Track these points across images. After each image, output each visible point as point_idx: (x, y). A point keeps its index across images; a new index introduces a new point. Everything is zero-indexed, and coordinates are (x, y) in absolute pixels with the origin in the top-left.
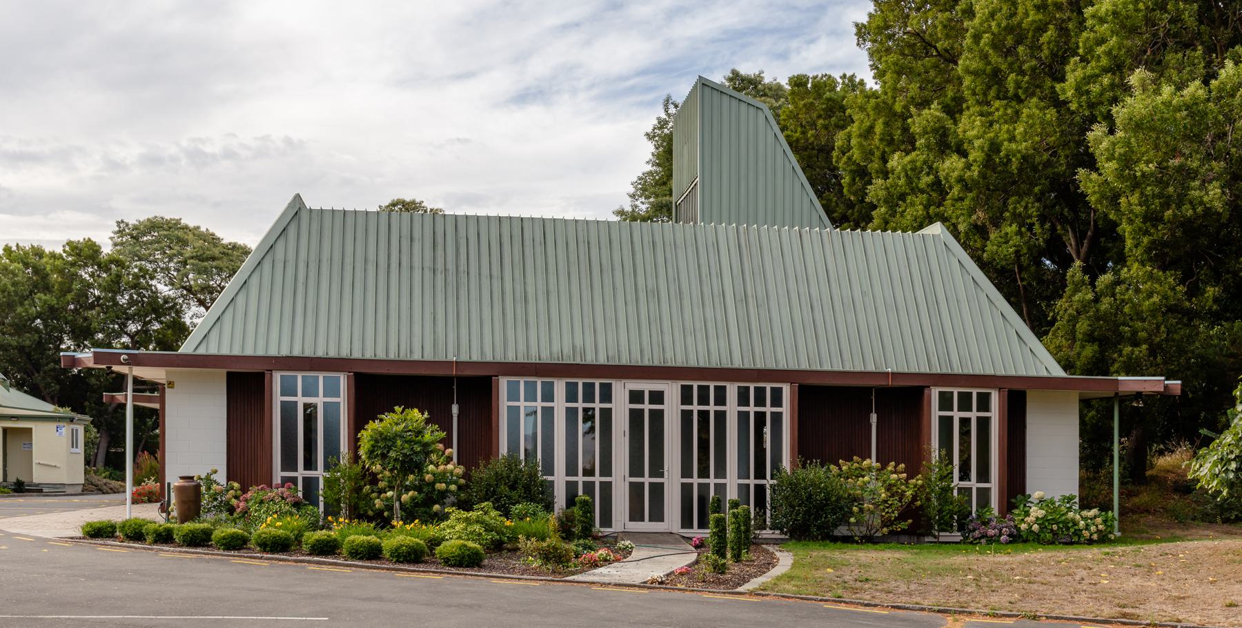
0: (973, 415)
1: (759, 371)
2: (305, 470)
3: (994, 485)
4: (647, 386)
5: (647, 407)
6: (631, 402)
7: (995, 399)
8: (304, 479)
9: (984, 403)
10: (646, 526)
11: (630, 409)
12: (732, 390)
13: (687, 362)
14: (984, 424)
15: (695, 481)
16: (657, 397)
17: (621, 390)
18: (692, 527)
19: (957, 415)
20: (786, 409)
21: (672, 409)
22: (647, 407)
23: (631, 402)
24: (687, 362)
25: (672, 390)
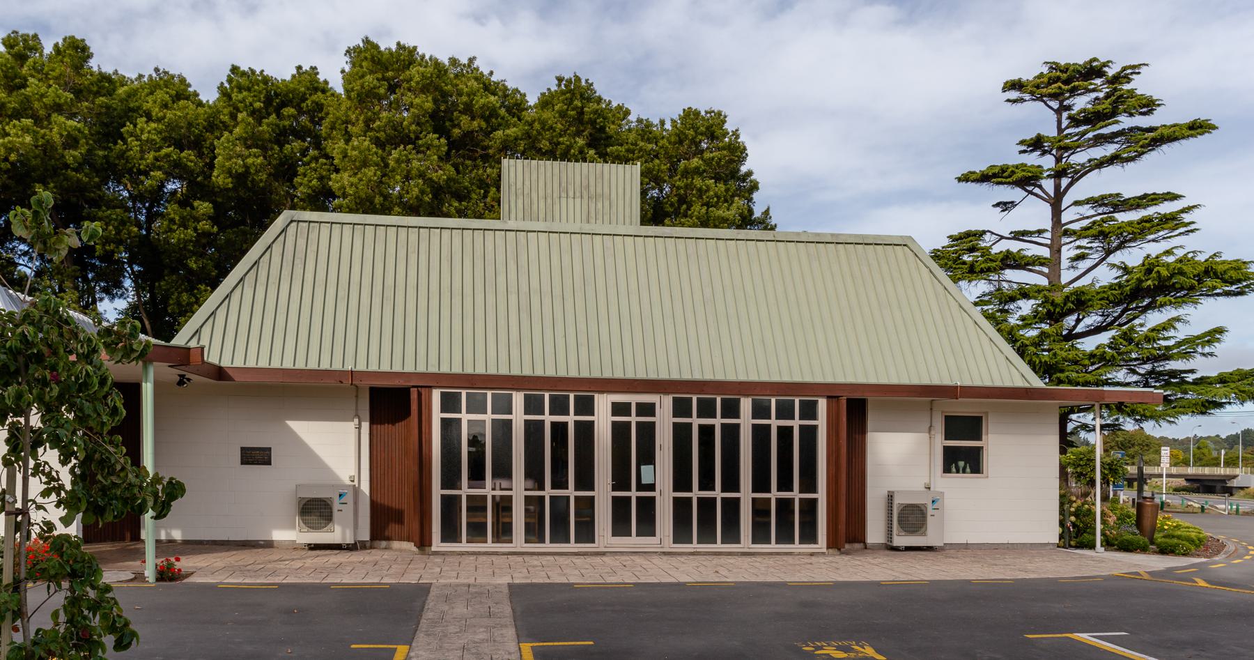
0: (717, 422)
1: (741, 383)
2: (778, 491)
3: (437, 492)
4: (633, 399)
5: (633, 419)
6: (614, 414)
7: (822, 404)
8: (551, 497)
9: (809, 410)
10: (634, 541)
11: (674, 423)
12: (746, 405)
13: (920, 378)
14: (809, 434)
15: (548, 492)
16: (646, 409)
17: (603, 403)
18: (544, 542)
19: (696, 422)
20: (821, 422)
21: (664, 421)
22: (633, 419)
23: (614, 414)
24: (920, 378)
25: (664, 405)
